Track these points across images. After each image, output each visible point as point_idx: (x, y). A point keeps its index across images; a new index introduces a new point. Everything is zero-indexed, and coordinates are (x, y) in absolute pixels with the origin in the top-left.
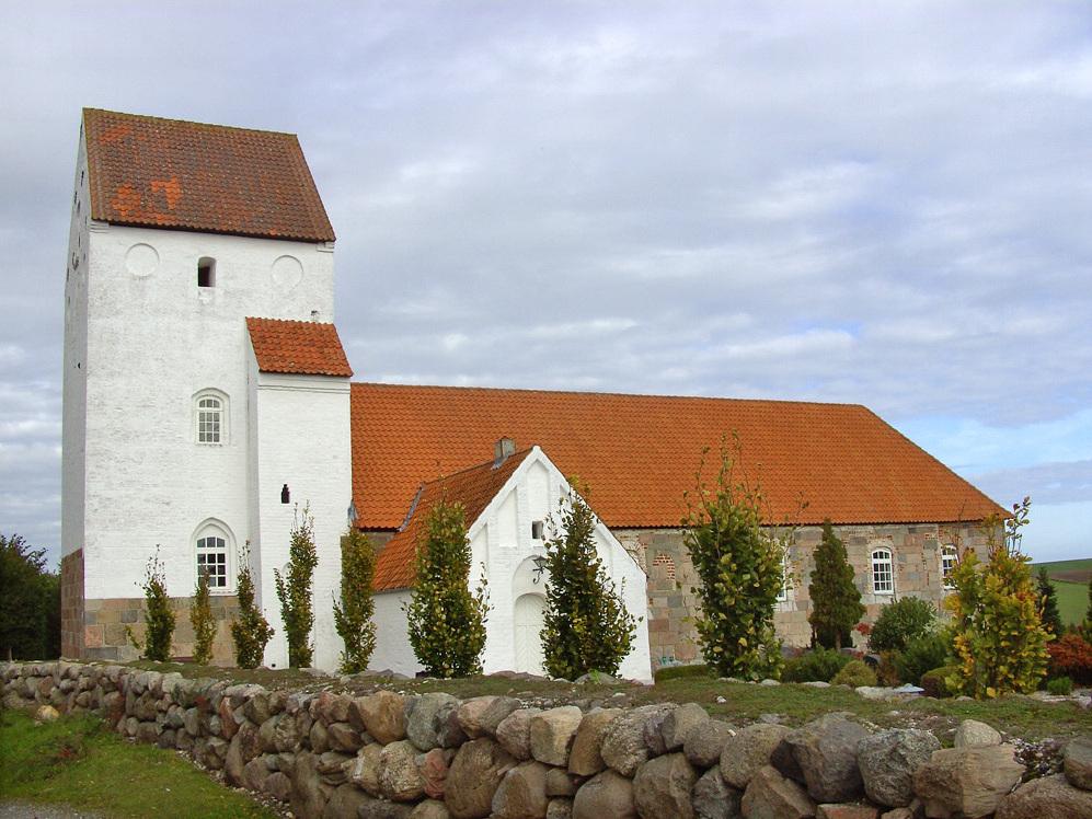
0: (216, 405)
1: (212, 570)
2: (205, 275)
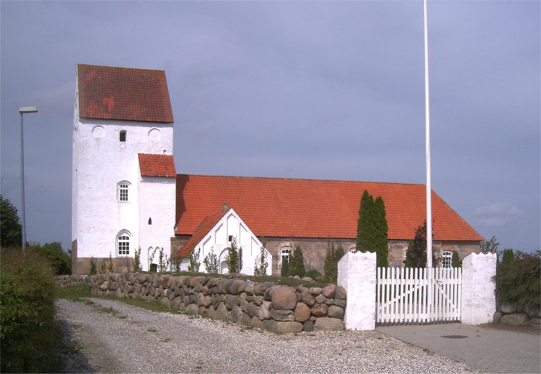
0: (127, 187)
1: (124, 248)
2: (123, 136)
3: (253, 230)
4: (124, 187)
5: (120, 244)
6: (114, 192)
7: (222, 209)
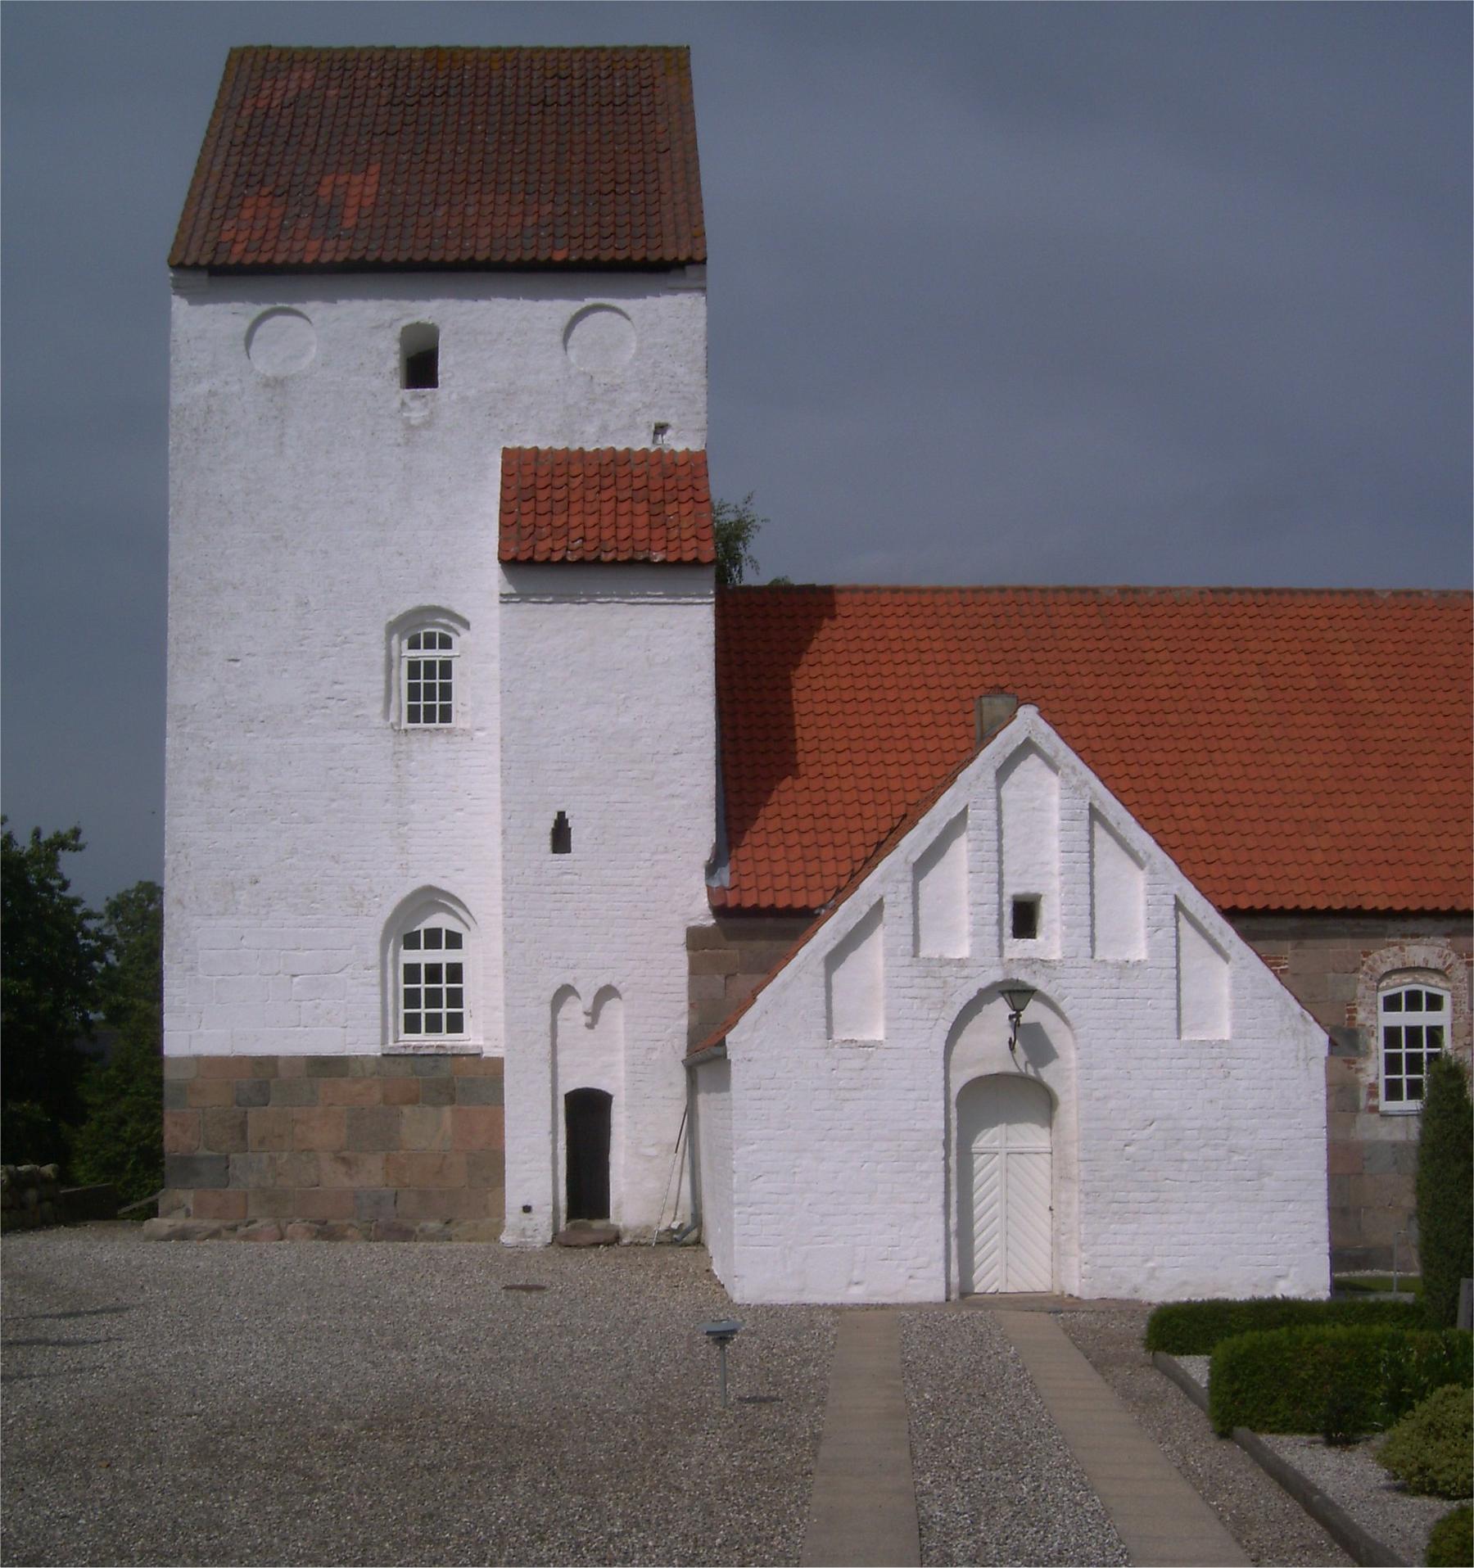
0: (446, 643)
1: (434, 999)
2: (420, 368)
3: (1124, 784)
4: (430, 645)
5: (411, 972)
6: (368, 673)
7: (973, 718)
